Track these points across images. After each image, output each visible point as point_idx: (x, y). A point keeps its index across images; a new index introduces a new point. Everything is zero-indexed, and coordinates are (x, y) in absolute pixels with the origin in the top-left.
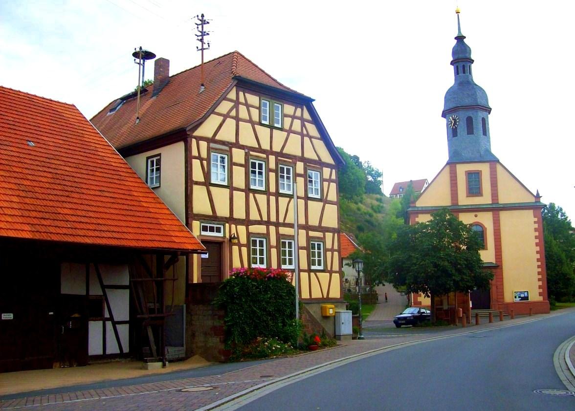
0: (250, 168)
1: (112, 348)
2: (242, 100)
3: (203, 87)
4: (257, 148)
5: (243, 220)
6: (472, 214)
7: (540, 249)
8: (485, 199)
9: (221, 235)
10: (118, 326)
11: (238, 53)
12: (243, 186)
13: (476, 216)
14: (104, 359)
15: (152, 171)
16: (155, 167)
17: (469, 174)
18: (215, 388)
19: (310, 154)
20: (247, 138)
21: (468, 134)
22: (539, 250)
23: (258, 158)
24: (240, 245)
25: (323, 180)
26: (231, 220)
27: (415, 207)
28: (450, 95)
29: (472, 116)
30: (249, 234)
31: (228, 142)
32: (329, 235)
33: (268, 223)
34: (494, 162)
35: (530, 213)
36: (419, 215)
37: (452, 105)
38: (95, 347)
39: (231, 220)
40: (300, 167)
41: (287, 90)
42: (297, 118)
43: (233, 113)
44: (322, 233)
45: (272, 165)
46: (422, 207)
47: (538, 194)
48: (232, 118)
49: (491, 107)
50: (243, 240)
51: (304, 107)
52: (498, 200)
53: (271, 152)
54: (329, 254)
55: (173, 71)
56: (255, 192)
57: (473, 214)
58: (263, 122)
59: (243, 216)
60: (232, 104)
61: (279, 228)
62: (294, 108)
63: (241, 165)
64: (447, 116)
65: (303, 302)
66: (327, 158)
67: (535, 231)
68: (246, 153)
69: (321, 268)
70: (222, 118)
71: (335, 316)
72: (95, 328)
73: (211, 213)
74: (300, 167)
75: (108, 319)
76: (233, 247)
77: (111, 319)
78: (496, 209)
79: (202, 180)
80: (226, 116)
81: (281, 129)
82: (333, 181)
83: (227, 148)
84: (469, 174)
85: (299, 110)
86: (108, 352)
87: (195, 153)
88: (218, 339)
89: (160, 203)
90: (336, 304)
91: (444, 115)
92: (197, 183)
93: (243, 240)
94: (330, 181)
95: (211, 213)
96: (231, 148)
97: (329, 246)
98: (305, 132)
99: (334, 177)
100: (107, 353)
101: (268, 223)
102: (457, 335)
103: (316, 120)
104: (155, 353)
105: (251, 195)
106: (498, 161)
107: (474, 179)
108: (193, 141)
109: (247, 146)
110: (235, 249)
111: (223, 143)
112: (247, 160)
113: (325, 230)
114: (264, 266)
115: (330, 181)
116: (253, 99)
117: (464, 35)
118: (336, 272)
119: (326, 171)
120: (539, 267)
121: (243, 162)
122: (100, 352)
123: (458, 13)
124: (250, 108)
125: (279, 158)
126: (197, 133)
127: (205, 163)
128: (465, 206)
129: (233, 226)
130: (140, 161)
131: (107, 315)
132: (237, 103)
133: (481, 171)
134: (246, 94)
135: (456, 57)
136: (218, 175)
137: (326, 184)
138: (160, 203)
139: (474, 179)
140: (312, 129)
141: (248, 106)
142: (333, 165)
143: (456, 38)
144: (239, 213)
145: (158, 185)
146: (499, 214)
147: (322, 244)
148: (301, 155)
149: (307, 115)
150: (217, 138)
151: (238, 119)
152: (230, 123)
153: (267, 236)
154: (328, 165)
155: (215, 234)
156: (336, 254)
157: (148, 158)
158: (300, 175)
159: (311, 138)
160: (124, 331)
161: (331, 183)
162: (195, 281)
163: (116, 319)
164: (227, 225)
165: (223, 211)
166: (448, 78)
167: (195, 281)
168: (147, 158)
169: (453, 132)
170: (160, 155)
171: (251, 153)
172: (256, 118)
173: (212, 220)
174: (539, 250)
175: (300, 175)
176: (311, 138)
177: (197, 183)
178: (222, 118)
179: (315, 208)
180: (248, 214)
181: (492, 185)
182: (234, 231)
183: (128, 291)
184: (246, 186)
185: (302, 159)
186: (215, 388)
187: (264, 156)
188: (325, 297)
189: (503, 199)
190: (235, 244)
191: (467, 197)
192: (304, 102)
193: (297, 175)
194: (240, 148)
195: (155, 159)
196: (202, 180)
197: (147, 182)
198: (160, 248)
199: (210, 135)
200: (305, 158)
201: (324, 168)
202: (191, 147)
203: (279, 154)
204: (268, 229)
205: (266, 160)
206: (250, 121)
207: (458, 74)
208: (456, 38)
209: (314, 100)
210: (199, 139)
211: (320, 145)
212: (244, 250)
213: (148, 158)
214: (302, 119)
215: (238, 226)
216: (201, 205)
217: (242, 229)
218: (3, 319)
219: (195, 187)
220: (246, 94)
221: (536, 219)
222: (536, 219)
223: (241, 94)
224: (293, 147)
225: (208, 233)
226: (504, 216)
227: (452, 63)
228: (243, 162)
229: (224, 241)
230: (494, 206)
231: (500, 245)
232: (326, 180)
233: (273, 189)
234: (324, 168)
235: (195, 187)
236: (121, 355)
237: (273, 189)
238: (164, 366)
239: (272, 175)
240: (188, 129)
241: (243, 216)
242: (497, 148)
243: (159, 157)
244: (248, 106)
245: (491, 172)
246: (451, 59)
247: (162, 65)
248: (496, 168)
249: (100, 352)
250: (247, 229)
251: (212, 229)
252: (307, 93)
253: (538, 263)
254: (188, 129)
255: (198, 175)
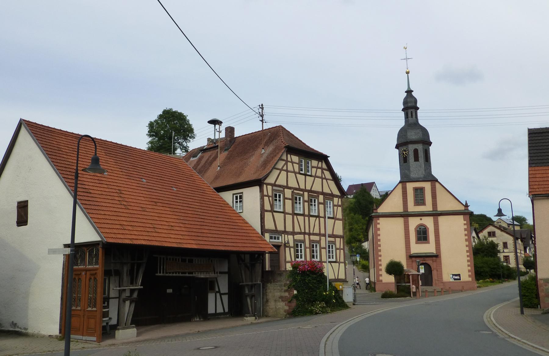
0: (294, 200)
1: (220, 310)
2: (289, 159)
3: (263, 150)
4: (298, 188)
5: (291, 232)
6: (418, 218)
7: (468, 233)
8: (428, 207)
9: (280, 240)
10: (223, 296)
11: (282, 127)
12: (291, 212)
13: (421, 219)
14: (216, 316)
15: (237, 202)
16: (238, 200)
17: (416, 190)
18: (316, 327)
19: (326, 190)
20: (293, 183)
21: (415, 161)
22: (468, 244)
23: (298, 194)
24: (290, 247)
25: (334, 206)
26: (285, 232)
27: (377, 212)
28: (402, 133)
29: (417, 148)
30: (295, 240)
31: (283, 186)
32: (338, 240)
33: (305, 233)
34: (434, 180)
35: (461, 217)
36: (380, 218)
37: (403, 141)
38: (211, 310)
39: (285, 232)
40: (321, 198)
41: (316, 153)
42: (319, 168)
43: (285, 168)
44: (334, 239)
45: (306, 198)
46: (382, 213)
47: (466, 203)
48: (284, 170)
49: (432, 142)
50: (291, 244)
51: (323, 161)
52: (437, 208)
53: (305, 190)
54: (338, 251)
55: (236, 135)
56: (297, 215)
57: (419, 218)
58: (301, 172)
59: (291, 230)
60: (284, 162)
61: (311, 236)
62: (317, 162)
63: (290, 199)
64: (399, 148)
65: (331, 281)
66: (336, 192)
67: (465, 236)
68: (292, 191)
69: (334, 260)
70: (279, 171)
71: (342, 290)
72: (211, 297)
73: (274, 229)
74: (321, 198)
75: (217, 292)
76: (286, 248)
77: (219, 292)
78: (436, 214)
79: (270, 209)
80: (281, 170)
81: (311, 176)
82: (340, 206)
83: (282, 189)
84: (416, 190)
85: (320, 163)
86: (218, 312)
87: (265, 193)
88: (284, 304)
89: (246, 223)
90: (343, 283)
91: (397, 147)
92: (267, 211)
93: (291, 244)
94: (338, 206)
95: (274, 229)
96: (284, 189)
97: (338, 246)
98: (323, 176)
99: (340, 203)
100: (217, 312)
101: (305, 233)
102: (405, 305)
103: (330, 168)
104: (251, 313)
105: (295, 217)
106: (437, 181)
107: (419, 194)
108: (264, 187)
109: (292, 187)
110: (287, 249)
111: (280, 186)
112: (292, 196)
113: (335, 236)
114: (303, 259)
115: (338, 206)
116: (295, 159)
117: (413, 90)
118: (342, 263)
119: (336, 200)
120: (468, 266)
121: (291, 197)
122: (214, 312)
123: (408, 73)
124: (294, 164)
125: (310, 193)
126: (266, 181)
127: (271, 198)
128: (413, 212)
129: (286, 236)
130: (228, 197)
131: (217, 290)
132: (287, 161)
133: (424, 187)
134: (291, 156)
135: (406, 106)
136: (278, 207)
137: (335, 208)
138: (246, 223)
139: (419, 194)
140: (328, 174)
141: (292, 162)
142: (339, 196)
143: (406, 92)
144: (289, 229)
145: (242, 211)
146: (438, 218)
147: (334, 245)
148: (321, 191)
149: (324, 166)
150: (277, 183)
151: (287, 171)
152: (284, 173)
153: (304, 241)
154: (337, 196)
155: (276, 241)
156: (342, 251)
157: (233, 194)
158: (321, 203)
159: (327, 179)
160: (225, 298)
161: (338, 207)
162: (267, 269)
163: (221, 292)
164: (283, 235)
165: (280, 228)
166: (400, 122)
167: (267, 269)
168: (233, 194)
169: (404, 160)
170: (242, 193)
171: (295, 191)
172: (297, 170)
173: (275, 232)
174: (468, 244)
175: (321, 203)
176: (327, 179)
177: (267, 211)
178: (279, 171)
179: (330, 222)
180: (263, 216)
181: (432, 197)
182: (286, 239)
183: (227, 276)
184: (292, 212)
185: (323, 193)
186: (316, 327)
187: (302, 193)
188: (336, 278)
189: (441, 208)
190: (287, 247)
191: (414, 206)
192: (323, 158)
193: (319, 203)
194: (289, 189)
195: (238, 195)
196: (270, 209)
197: (233, 207)
198: (253, 251)
199: (273, 182)
200: (324, 192)
201: (334, 198)
202: (263, 189)
203: (310, 191)
204: (304, 237)
205: (303, 195)
206: (294, 172)
207: (407, 118)
208: (406, 92)
209: (329, 157)
210: (268, 184)
211: (332, 184)
212: (292, 250)
213: (233, 194)
214: (322, 169)
215: (289, 236)
216: (269, 224)
217: (291, 237)
218: (167, 292)
219: (266, 213)
220: (291, 156)
221: (465, 222)
222: (465, 222)
223: (289, 156)
224: (317, 187)
225: (273, 240)
226: (442, 220)
227: (403, 110)
228: (291, 197)
229: (282, 245)
230: (434, 213)
231: (439, 241)
232: (336, 206)
233: (307, 213)
234: (334, 198)
235: (266, 213)
236: (224, 313)
237: (307, 213)
238: (256, 319)
239: (306, 204)
240: (262, 180)
241: (291, 230)
242: (435, 172)
243: (242, 194)
244: (292, 162)
245: (432, 188)
246: (403, 107)
247: (230, 130)
248: (435, 185)
249: (214, 312)
250: (294, 237)
251: (275, 238)
252: (325, 152)
253: (468, 258)
254: (262, 180)
255: (267, 207)
